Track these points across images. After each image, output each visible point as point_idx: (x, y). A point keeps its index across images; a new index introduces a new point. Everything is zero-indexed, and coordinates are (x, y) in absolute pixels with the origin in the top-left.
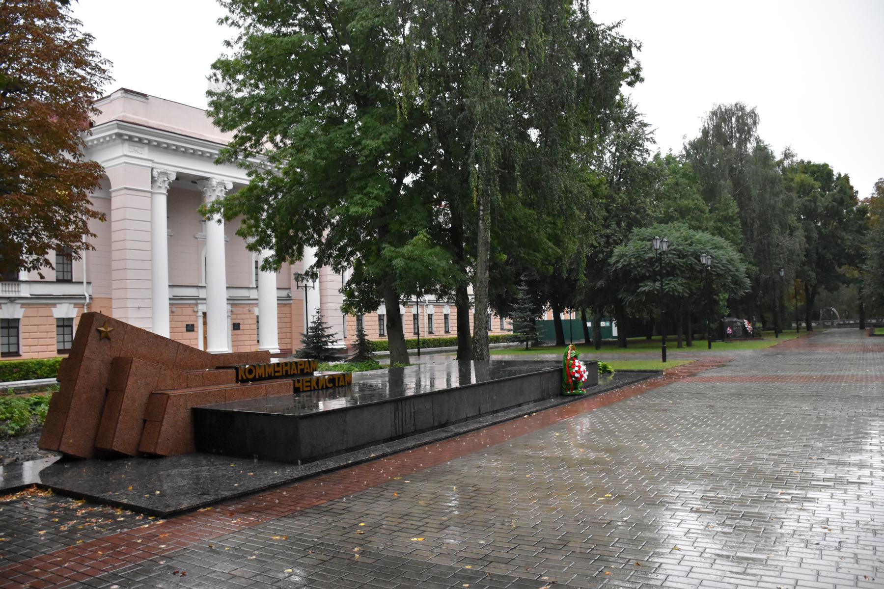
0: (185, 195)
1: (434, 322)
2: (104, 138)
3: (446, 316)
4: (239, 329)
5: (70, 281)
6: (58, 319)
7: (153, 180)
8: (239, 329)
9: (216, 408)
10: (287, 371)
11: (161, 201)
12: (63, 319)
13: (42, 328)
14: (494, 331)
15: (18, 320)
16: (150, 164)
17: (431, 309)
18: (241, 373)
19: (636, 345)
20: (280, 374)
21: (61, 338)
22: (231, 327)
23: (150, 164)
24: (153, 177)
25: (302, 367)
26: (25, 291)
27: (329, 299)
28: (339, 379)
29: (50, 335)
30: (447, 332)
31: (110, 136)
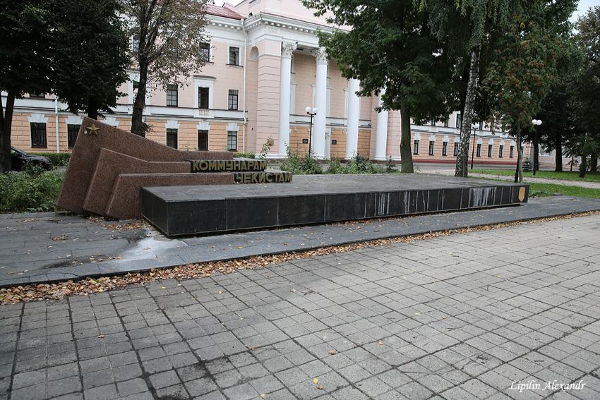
0: (302, 57)
1: (503, 150)
2: (255, 24)
3: (512, 148)
4: (336, 144)
5: (176, 106)
6: (229, 132)
7: (283, 49)
8: (336, 144)
9: (187, 187)
10: (237, 168)
11: (287, 62)
12: (172, 130)
13: (190, 135)
14: (504, 158)
15: (207, 131)
16: (281, 39)
17: (502, 143)
18: (195, 165)
19: (459, 178)
20: (232, 169)
21: (230, 143)
22: (330, 142)
23: (281, 39)
24: (282, 48)
25: (252, 165)
26: (437, 130)
27: (394, 129)
28: (279, 176)
29: (224, 140)
30: (511, 157)
31: (258, 22)
